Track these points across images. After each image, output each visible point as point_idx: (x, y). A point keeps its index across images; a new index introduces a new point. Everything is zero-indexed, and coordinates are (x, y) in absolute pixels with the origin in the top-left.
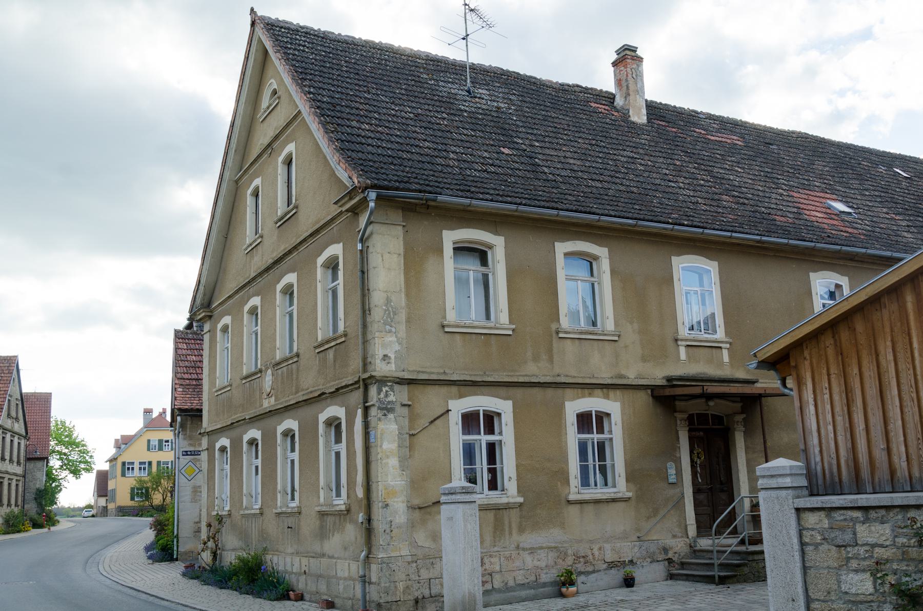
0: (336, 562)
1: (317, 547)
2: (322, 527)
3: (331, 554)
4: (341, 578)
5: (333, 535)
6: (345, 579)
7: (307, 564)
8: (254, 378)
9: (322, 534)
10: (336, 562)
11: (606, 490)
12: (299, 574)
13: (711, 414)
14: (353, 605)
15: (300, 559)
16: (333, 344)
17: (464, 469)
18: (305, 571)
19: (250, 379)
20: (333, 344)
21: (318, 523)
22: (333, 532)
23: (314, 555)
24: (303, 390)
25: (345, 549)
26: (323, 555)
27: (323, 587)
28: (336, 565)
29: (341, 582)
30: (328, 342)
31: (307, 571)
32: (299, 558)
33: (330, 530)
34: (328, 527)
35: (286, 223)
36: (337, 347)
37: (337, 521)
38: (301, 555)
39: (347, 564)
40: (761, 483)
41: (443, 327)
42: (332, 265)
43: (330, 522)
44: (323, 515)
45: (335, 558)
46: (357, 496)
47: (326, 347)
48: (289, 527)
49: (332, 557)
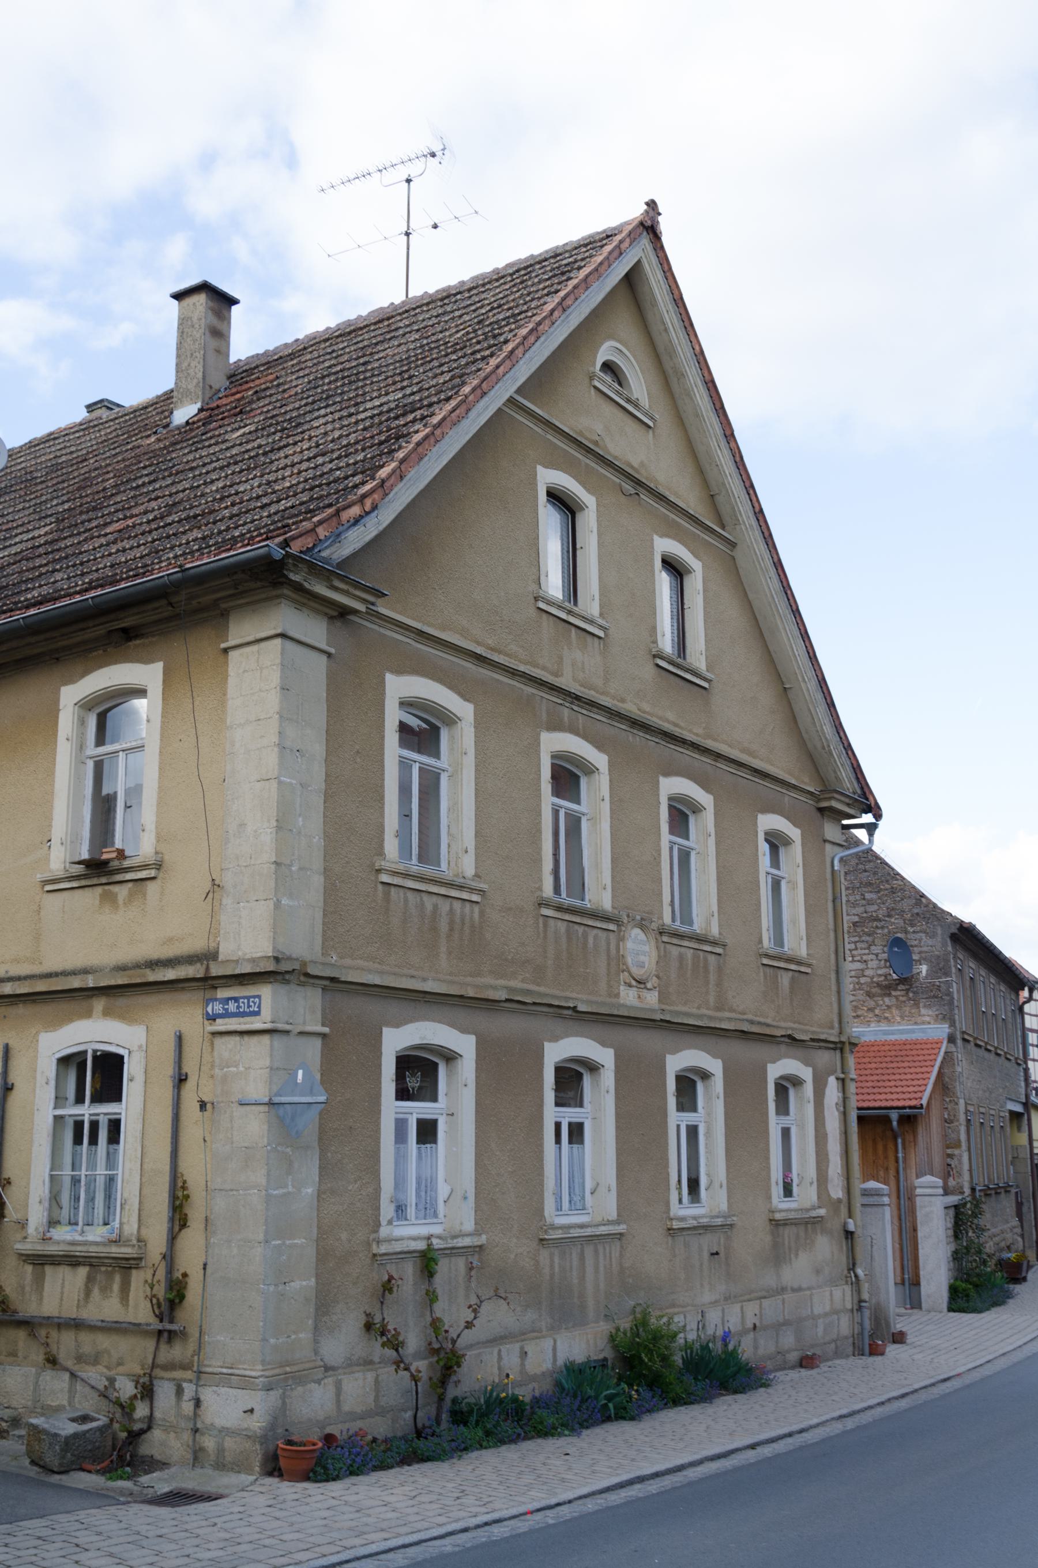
0: (811, 1295)
1: (770, 1280)
2: (776, 1246)
3: (796, 1286)
4: (819, 1316)
5: (797, 1255)
6: (826, 1315)
7: (757, 1312)
8: (590, 923)
9: (778, 1256)
10: (811, 1295)
11: (858, 1205)
12: (744, 1332)
13: (518, 391)
14: (837, 1347)
15: (742, 1307)
16: (793, 967)
17: (85, 1052)
18: (755, 1325)
19: (578, 919)
20: (793, 967)
21: (768, 1239)
22: (797, 1251)
23: (764, 1293)
24: (732, 1010)
25: (818, 1272)
26: (783, 1290)
27: (788, 1340)
28: (811, 1299)
29: (820, 1321)
30: (789, 960)
31: (758, 1324)
32: (739, 1305)
33: (790, 1248)
34: (786, 1243)
35: (677, 680)
36: (796, 974)
37: (802, 1234)
38: (741, 1298)
39: (827, 1294)
40: (589, 1251)
41: (536, 599)
42: (776, 842)
43: (789, 1237)
44: (777, 1225)
45: (805, 1290)
46: (829, 1195)
47: (782, 965)
48: (717, 1253)
49: (800, 1289)
